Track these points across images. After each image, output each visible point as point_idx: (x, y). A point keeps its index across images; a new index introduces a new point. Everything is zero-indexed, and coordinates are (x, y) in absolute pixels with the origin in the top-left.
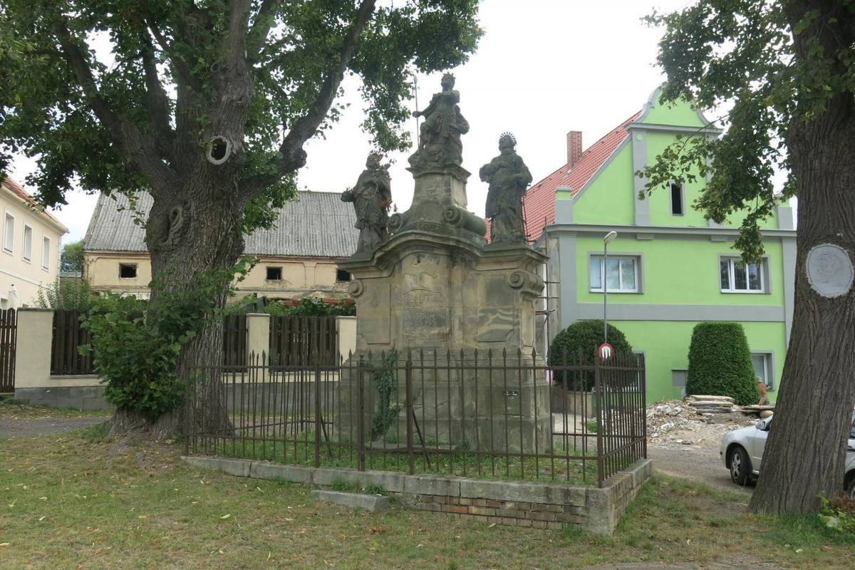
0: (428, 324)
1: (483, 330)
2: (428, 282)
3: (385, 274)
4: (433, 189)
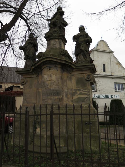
0: (53, 95)
1: (75, 97)
2: (54, 78)
3: (35, 76)
4: (55, 44)
